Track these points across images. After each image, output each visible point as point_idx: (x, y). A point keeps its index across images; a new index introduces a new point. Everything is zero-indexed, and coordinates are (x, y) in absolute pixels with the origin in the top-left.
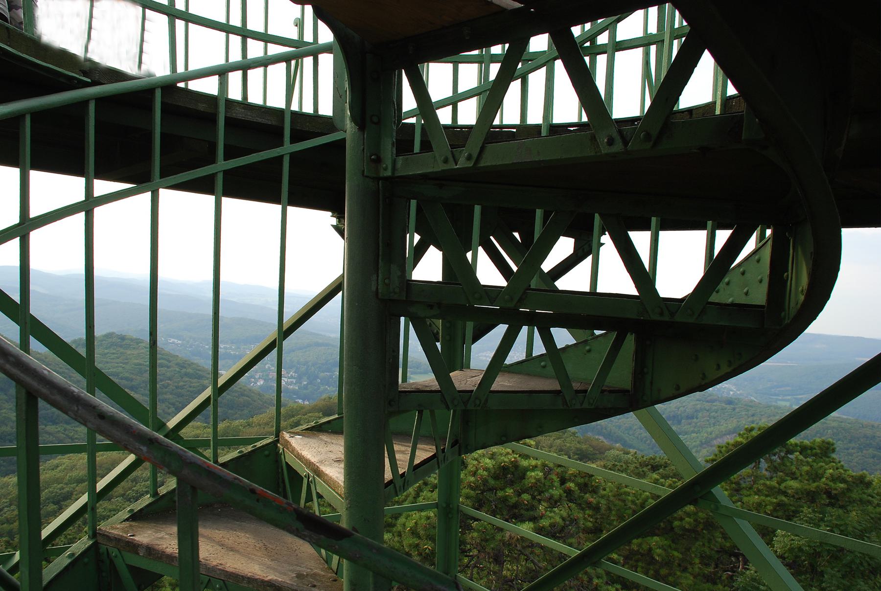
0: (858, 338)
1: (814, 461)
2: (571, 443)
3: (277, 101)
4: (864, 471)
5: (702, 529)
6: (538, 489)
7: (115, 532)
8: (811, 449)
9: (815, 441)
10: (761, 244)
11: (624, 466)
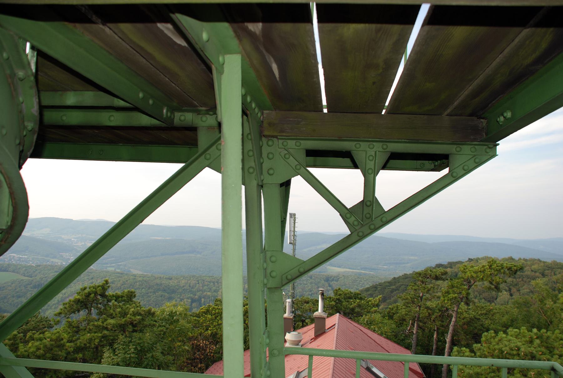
0: (152, 225)
1: (124, 304)
8: (122, 297)
9: (124, 291)
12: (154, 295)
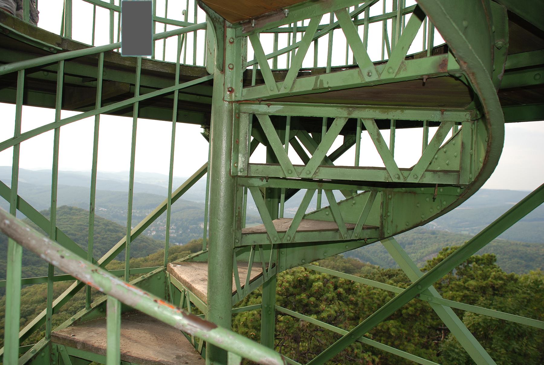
2: (340, 263)
3: (171, 58)
4: (513, 272)
5: (420, 314)
6: (319, 295)
7: (63, 334)
8: (482, 260)
9: (484, 255)
10: (455, 134)
11: (372, 277)
12: (510, 261)
